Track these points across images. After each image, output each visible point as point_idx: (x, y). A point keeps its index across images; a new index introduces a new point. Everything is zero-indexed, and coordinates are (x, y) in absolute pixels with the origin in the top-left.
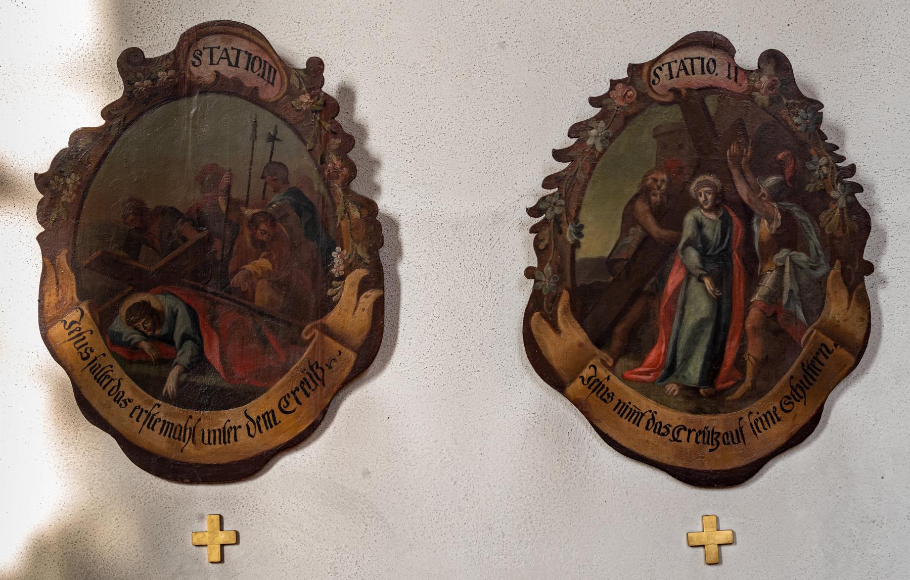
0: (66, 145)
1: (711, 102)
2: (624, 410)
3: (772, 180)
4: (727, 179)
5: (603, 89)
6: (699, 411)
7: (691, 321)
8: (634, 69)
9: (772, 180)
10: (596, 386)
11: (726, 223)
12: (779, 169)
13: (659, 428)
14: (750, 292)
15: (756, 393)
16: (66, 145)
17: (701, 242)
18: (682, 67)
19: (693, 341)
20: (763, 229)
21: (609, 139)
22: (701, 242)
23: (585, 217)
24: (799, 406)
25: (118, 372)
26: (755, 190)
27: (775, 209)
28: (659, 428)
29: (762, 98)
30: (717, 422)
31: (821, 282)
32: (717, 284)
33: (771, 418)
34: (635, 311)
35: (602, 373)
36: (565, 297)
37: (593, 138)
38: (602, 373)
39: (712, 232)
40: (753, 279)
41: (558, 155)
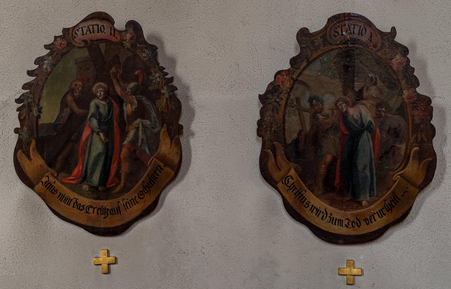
2: (62, 197)
3: (132, 85)
6: (98, 198)
7: (94, 154)
9: (132, 85)
10: (49, 186)
11: (110, 106)
13: (79, 207)
14: (123, 140)
15: (125, 190)
17: (98, 115)
19: (95, 164)
20: (128, 109)
24: (147, 196)
26: (124, 89)
28: (79, 207)
29: (127, 45)
30: (106, 204)
31: (158, 134)
33: (133, 202)
35: (52, 179)
36: (33, 143)
38: (52, 179)
39: (103, 110)
40: (124, 134)
41: (30, 73)
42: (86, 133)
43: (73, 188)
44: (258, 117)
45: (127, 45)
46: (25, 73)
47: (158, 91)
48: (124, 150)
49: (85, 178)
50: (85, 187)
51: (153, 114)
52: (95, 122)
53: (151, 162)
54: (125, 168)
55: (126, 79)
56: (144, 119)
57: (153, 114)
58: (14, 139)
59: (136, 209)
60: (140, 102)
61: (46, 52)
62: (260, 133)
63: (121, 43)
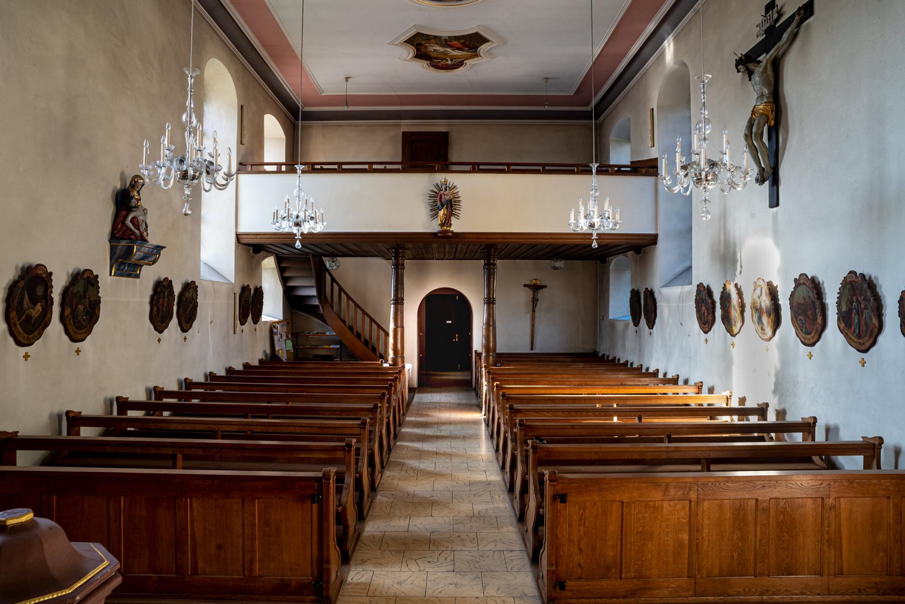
0: (98, 280)
1: (853, 283)
2: (851, 339)
3: (863, 297)
4: (857, 297)
5: (841, 282)
6: (859, 339)
7: (856, 322)
8: (844, 278)
9: (863, 297)
10: (846, 333)
11: (858, 304)
12: (863, 295)
13: (854, 341)
14: (862, 318)
15: (865, 336)
16: (98, 280)
17: (855, 308)
18: (501, 249)
19: (857, 325)
20: (863, 306)
21: (843, 290)
22: (855, 308)
23: (842, 304)
24: (871, 339)
25: (799, 329)
26: (861, 299)
27: (863, 302)
28: (854, 341)
29: (860, 282)
30: (861, 341)
31: (871, 316)
32: (858, 316)
33: (867, 341)
34: (849, 321)
35: (847, 331)
36: (841, 318)
37: (842, 289)
38: (847, 331)
39: (856, 306)
40: (862, 315)
41: (838, 293)
42: (853, 315)
43: (852, 334)
44: (898, 310)
45: (860, 282)
46: (686, 377)
47: (869, 299)
48: (863, 321)
49: (855, 331)
50: (855, 335)
51: (869, 308)
52: (855, 311)
53: (871, 326)
54: (864, 329)
55: (861, 295)
56: (446, 167)
57: (869, 308)
58: (836, 316)
59: (868, 344)
60: (865, 304)
61: (841, 285)
62: (900, 316)
63: (858, 282)
